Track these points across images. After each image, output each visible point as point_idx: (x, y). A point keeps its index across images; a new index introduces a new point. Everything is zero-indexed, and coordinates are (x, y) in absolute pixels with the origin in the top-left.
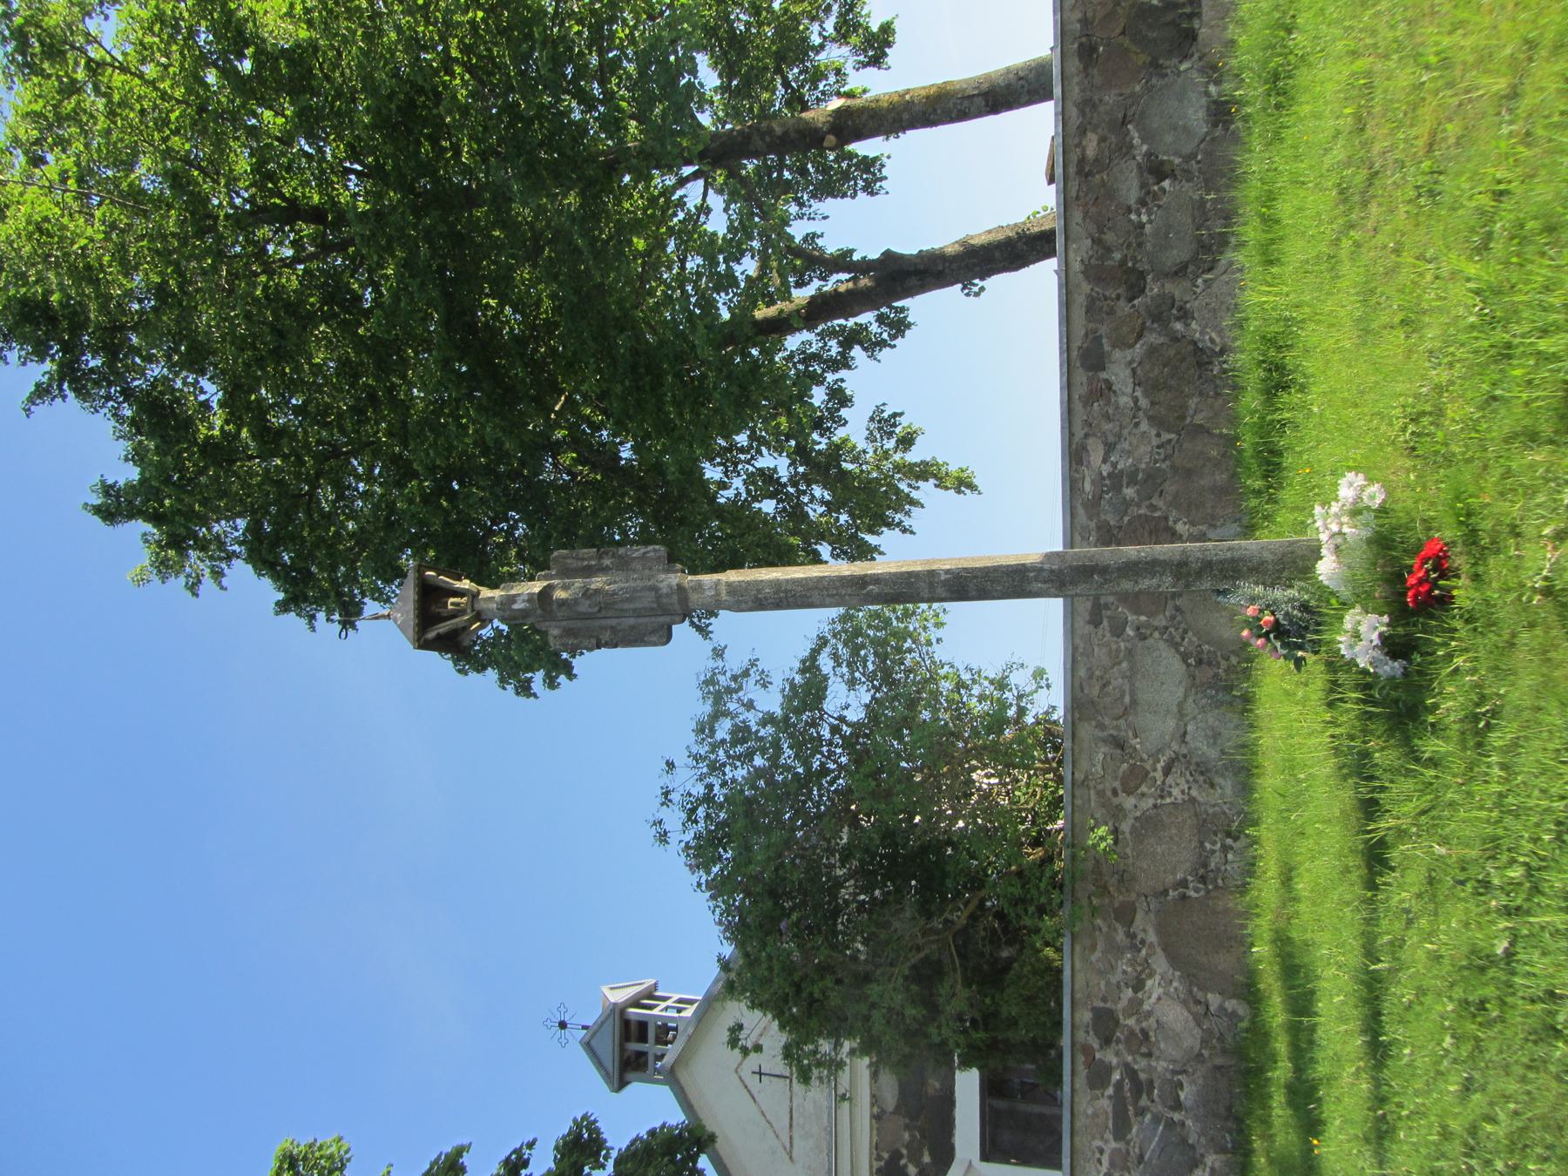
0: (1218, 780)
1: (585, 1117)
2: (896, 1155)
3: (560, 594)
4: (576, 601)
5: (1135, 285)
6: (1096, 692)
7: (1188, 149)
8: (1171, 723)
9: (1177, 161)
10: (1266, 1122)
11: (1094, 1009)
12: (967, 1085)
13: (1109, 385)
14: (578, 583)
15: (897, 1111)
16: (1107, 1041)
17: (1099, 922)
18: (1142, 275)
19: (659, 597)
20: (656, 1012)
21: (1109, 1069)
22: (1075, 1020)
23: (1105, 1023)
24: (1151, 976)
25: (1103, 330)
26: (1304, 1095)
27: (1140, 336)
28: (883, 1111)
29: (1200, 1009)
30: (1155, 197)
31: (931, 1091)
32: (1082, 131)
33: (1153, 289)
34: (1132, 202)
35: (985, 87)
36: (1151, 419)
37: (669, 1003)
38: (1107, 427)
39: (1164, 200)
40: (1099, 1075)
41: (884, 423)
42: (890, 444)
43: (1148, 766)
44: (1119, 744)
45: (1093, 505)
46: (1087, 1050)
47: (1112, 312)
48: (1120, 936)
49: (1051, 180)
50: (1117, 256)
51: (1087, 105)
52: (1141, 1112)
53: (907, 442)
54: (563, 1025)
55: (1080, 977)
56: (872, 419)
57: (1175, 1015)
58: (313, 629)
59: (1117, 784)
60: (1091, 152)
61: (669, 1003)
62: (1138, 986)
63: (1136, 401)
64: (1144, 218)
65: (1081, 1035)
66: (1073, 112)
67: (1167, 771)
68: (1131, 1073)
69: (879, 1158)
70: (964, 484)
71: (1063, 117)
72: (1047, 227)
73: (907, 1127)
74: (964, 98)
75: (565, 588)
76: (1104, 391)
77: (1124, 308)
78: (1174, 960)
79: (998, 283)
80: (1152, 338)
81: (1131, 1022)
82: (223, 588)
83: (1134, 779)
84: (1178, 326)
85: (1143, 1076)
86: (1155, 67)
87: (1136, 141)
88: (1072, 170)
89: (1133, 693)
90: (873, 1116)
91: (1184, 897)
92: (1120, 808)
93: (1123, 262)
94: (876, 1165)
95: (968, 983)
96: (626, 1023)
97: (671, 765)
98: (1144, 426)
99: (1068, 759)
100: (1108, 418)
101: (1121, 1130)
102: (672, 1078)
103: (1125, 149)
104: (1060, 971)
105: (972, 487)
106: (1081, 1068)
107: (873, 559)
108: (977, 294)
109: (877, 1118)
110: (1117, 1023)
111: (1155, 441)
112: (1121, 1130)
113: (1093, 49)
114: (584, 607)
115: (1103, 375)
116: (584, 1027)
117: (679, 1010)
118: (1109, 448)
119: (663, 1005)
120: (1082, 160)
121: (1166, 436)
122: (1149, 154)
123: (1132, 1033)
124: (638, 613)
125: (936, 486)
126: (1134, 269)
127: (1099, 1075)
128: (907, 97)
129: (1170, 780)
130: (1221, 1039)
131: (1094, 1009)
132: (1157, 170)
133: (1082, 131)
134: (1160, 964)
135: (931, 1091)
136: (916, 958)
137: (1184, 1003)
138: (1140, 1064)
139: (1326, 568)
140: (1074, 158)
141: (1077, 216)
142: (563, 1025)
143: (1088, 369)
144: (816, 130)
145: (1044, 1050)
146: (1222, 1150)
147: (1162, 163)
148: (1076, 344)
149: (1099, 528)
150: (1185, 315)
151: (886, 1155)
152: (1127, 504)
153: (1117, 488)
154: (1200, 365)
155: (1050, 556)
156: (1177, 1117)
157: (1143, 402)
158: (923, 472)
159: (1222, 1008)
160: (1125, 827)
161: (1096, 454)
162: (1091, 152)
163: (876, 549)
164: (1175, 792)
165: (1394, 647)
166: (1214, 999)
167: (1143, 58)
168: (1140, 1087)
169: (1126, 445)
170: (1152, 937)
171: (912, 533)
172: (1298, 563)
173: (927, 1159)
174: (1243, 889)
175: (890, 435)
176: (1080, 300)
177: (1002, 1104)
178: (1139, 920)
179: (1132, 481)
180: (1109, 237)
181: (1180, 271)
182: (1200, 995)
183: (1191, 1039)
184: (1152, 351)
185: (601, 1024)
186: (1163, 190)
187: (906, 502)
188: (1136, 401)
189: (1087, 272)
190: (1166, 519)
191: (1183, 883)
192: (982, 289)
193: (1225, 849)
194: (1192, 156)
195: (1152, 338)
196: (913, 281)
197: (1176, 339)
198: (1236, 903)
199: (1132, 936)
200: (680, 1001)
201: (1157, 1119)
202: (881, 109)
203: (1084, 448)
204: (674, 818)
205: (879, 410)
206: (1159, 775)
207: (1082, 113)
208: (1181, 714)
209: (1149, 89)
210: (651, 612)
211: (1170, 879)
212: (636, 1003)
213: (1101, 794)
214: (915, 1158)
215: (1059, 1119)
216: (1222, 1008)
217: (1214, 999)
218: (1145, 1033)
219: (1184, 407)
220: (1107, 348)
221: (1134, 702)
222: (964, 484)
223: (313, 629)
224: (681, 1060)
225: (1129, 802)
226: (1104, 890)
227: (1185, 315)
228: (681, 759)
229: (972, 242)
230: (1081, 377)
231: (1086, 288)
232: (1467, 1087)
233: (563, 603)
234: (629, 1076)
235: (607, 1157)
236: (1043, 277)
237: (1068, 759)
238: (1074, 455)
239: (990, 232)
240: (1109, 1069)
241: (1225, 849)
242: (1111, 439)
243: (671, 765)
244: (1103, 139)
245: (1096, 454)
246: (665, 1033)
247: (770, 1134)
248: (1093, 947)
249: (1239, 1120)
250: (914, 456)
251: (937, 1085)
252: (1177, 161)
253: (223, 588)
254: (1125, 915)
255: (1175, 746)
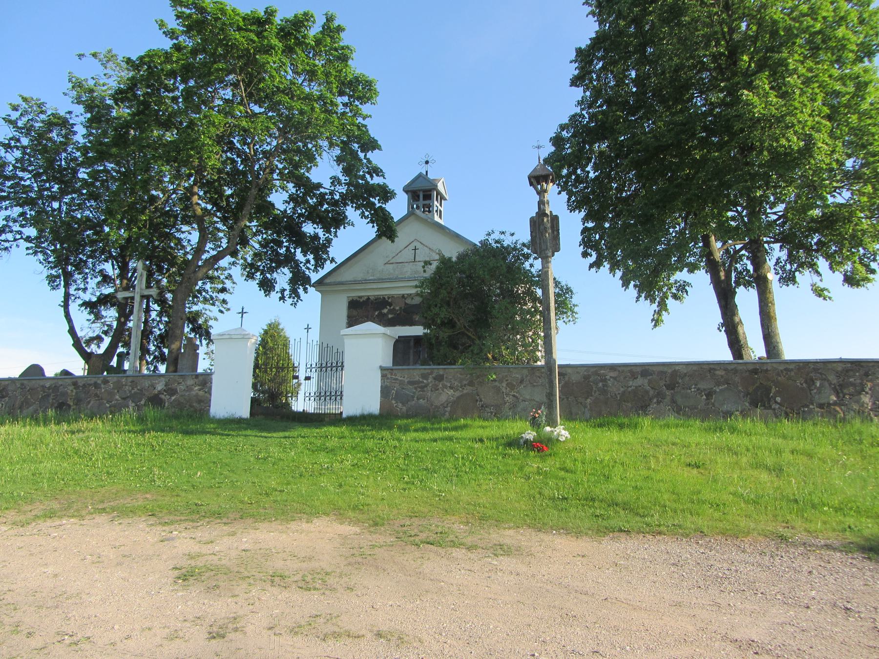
0: (511, 410)
1: (395, 194)
2: (390, 304)
3: (545, 220)
4: (543, 225)
5: (671, 387)
6: (538, 374)
7: (716, 405)
8: (528, 397)
9: (713, 401)
10: (416, 422)
11: (443, 375)
12: (418, 331)
13: (636, 378)
14: (549, 225)
15: (406, 304)
16: (435, 379)
17: (469, 376)
18: (673, 389)
19: (544, 250)
20: (436, 203)
21: (427, 379)
22: (439, 369)
23: (440, 378)
24: (454, 391)
25: (655, 377)
26: (424, 429)
27: (652, 388)
28: (405, 299)
29: (445, 405)
30: (700, 394)
31: (414, 317)
32: (726, 370)
33: (668, 393)
34: (699, 386)
35: (772, 334)
36: (624, 392)
37: (439, 207)
38: (622, 377)
39: (698, 396)
40: (425, 376)
41: (683, 287)
42: (674, 290)
43: (515, 390)
44: (522, 382)
45: (596, 373)
46: (431, 373)
47: (661, 379)
48: (465, 382)
49: (759, 358)
50: (680, 381)
51: (735, 371)
52: (416, 388)
53: (675, 297)
54: (427, 162)
55: (452, 370)
56: (685, 282)
57: (443, 398)
58: (571, 62)
59: (509, 381)
60: (717, 372)
61: (439, 207)
62: (451, 388)
63: (631, 387)
64: (693, 390)
65: (436, 371)
66: (733, 367)
67: (514, 396)
68: (426, 386)
69: (389, 298)
70: (656, 322)
71: (729, 363)
72: (744, 356)
73: (401, 308)
74: (768, 326)
75: (548, 220)
76: (634, 376)
77: (662, 383)
78: (458, 398)
79: (723, 337)
80: (651, 392)
81: (441, 386)
82: (587, 16)
83: (511, 386)
84: (655, 400)
85: (426, 389)
86: (747, 394)
87: (721, 387)
88: (712, 366)
89: (537, 386)
90: (403, 295)
91: (477, 401)
92: (502, 382)
93: (678, 383)
94: (386, 297)
95: (449, 337)
96: (430, 190)
97: (512, 235)
98: (622, 389)
99: (517, 366)
100: (625, 378)
101: (410, 383)
102: (411, 214)
103: (718, 384)
104: (454, 364)
105: (655, 326)
106: (427, 371)
107: (623, 287)
108: (719, 329)
109: (403, 296)
110: (440, 381)
111: (617, 393)
112: (410, 383)
113: (756, 374)
114: (542, 227)
115: (639, 376)
116: (427, 172)
117: (437, 211)
118: (615, 378)
119: (438, 205)
120: (715, 370)
121: (618, 396)
122: (715, 392)
123: (438, 386)
124: (540, 244)
125: (655, 311)
126: (675, 386)
127: (425, 376)
128: (770, 305)
129: (511, 397)
130: (438, 411)
131: (443, 375)
132: (709, 395)
133: (726, 370)
134: (458, 394)
135: (414, 317)
136: (456, 319)
137: (447, 401)
138: (429, 388)
139: (548, 429)
140: (716, 367)
141: (695, 368)
142: (427, 162)
143: (642, 372)
144: (759, 270)
145: (432, 359)
146: (407, 411)
147: (712, 396)
148: (650, 368)
149: (589, 375)
150: (658, 403)
151: (390, 301)
152: (597, 384)
153: (602, 381)
154: (642, 407)
155: (555, 361)
156: (415, 399)
157: (630, 389)
158: (663, 306)
159: (446, 412)
160: (497, 384)
161: (613, 374)
162: (717, 372)
163: (627, 287)
164: (508, 398)
165: (526, 442)
166: (448, 409)
167: (751, 390)
168: (422, 388)
169: (616, 383)
170: (465, 391)
171: (636, 301)
172: (552, 423)
173: (390, 316)
174: (480, 417)
175: (678, 290)
176: (665, 369)
177: (412, 343)
178: (469, 388)
179: (604, 386)
180: (687, 378)
181: (673, 401)
182: (449, 405)
183: (437, 403)
184: (647, 392)
185: (429, 181)
186: (702, 396)
187: (651, 298)
188: (631, 387)
189: (675, 371)
190: (592, 396)
191: (481, 401)
192: (721, 331)
193: (491, 413)
194: (714, 406)
195: (651, 392)
196: (723, 303)
197: (651, 400)
198: (476, 415)
199: (465, 385)
200: (440, 211)
201: (414, 393)
202: (766, 294)
203: (615, 370)
204: (496, 236)
205: (689, 284)
206: (512, 393)
207: (732, 370)
208: (531, 400)
209: (740, 391)
210: (540, 248)
211: (482, 397)
212: (439, 193)
213: (506, 376)
214: (390, 311)
215: (409, 365)
216: (446, 412)
217: (448, 409)
218: (438, 389)
219: (628, 402)
220: (648, 378)
221: (534, 386)
222: (656, 322)
223: (571, 62)
224: (418, 218)
225: (504, 385)
226: (478, 377)
227: (658, 403)
228: (514, 238)
229: (739, 327)
230: (639, 369)
231: (670, 371)
232: (427, 451)
233: (543, 220)
234: (410, 194)
235: (382, 203)
236: (726, 355)
237: (517, 366)
238: (613, 367)
239: (744, 333)
240: (427, 379)
241: (491, 413)
242: (618, 379)
243: (512, 235)
244: (722, 376)
245: (613, 374)
246: (428, 208)
247: (394, 255)
248: (461, 374)
249: (416, 416)
250: (670, 302)
251: (417, 319)
252: (713, 401)
253: (587, 16)
254: (471, 384)
255: (521, 398)
